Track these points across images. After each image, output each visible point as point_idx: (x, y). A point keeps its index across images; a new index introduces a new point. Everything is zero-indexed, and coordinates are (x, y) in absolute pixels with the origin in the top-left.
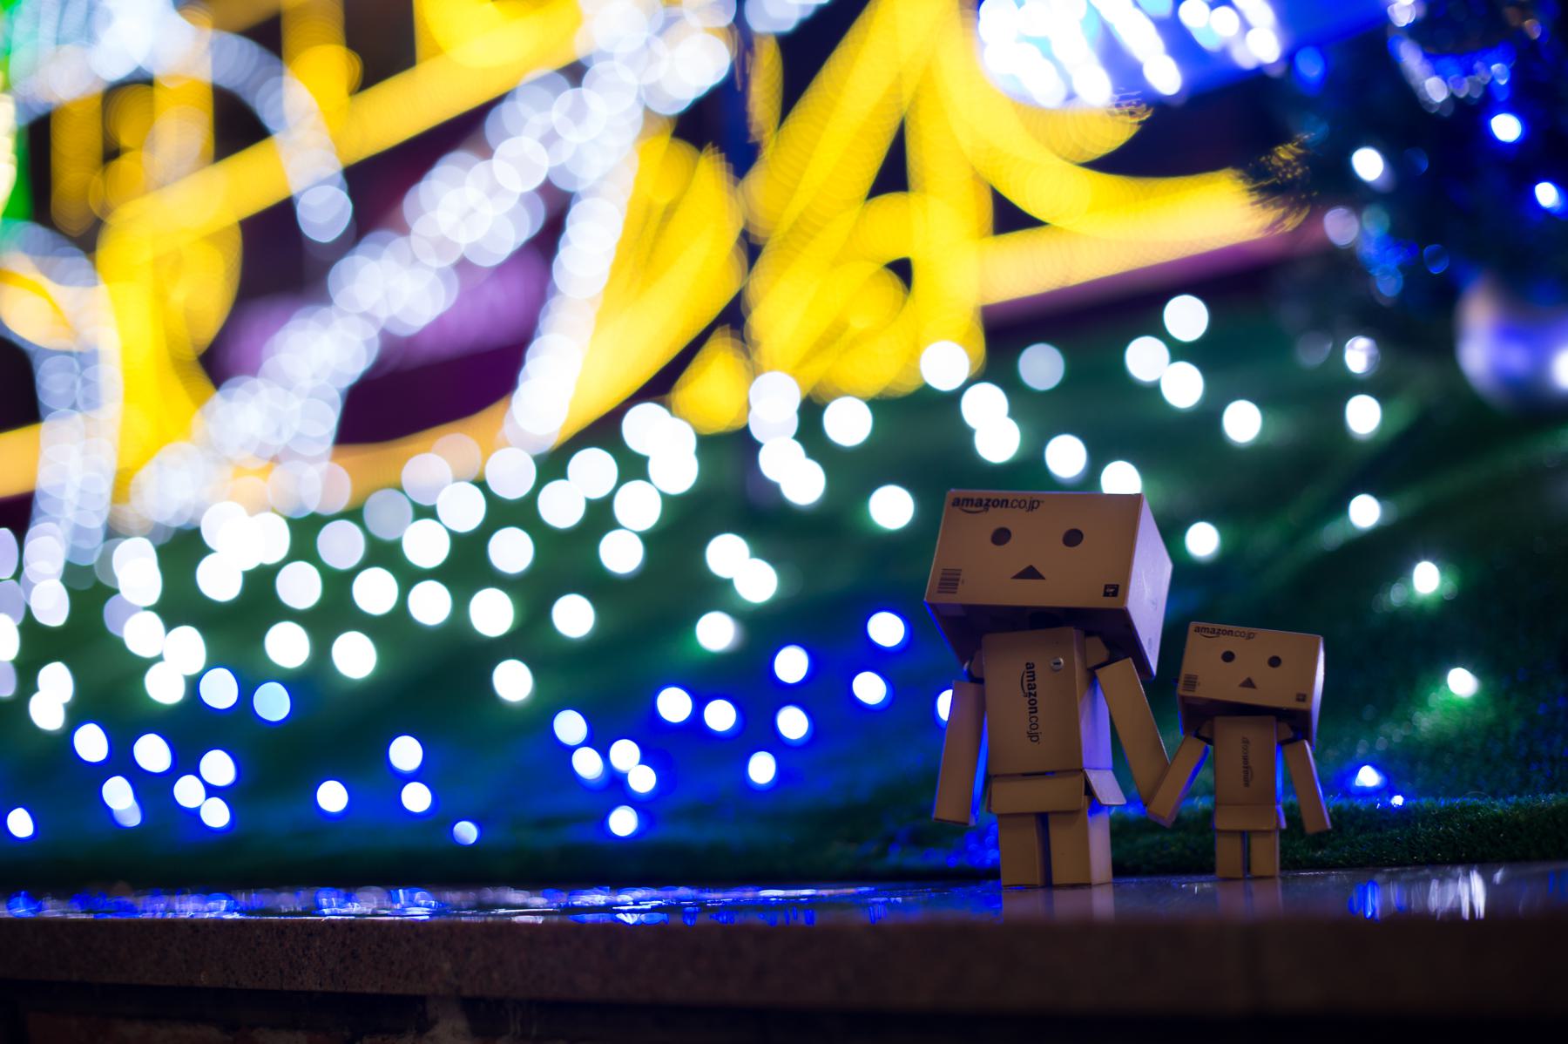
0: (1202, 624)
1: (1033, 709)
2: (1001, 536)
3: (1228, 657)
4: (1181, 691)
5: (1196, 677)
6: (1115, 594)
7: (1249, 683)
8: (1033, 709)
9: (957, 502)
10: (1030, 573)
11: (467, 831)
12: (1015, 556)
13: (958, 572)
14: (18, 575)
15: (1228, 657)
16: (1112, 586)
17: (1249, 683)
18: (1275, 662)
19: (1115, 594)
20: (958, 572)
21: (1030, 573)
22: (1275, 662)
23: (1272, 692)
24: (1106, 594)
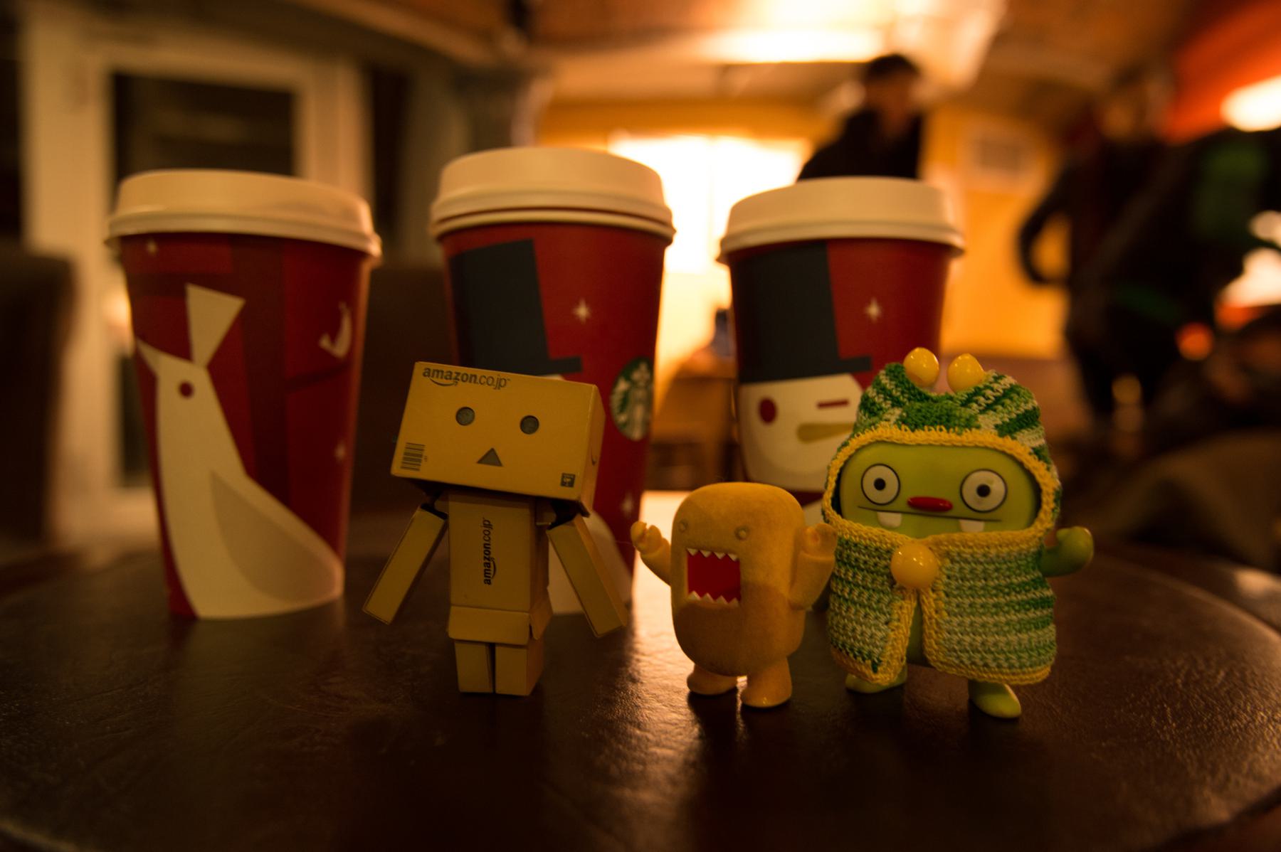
1: (487, 548)
2: (465, 416)
4: (397, 469)
7: (491, 458)
8: (487, 548)
13: (421, 448)
19: (571, 484)
20: (421, 448)
24: (563, 484)
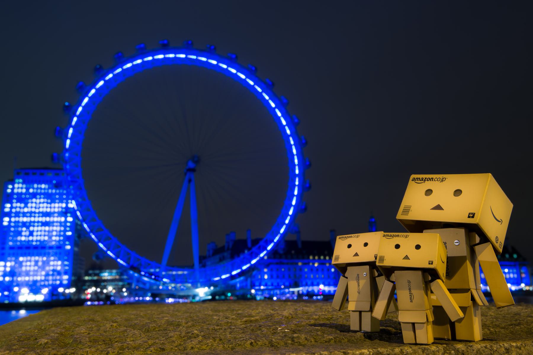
0: (341, 236)
1: (359, 286)
3: (397, 246)
5: (384, 257)
6: (473, 217)
7: (406, 258)
8: (359, 286)
9: (414, 179)
10: (438, 207)
11: (67, 155)
12: (433, 201)
14: (445, 243)
15: (397, 246)
16: (472, 214)
17: (406, 258)
18: (418, 247)
21: (438, 207)
22: (418, 247)
23: (419, 260)
24: (469, 217)
